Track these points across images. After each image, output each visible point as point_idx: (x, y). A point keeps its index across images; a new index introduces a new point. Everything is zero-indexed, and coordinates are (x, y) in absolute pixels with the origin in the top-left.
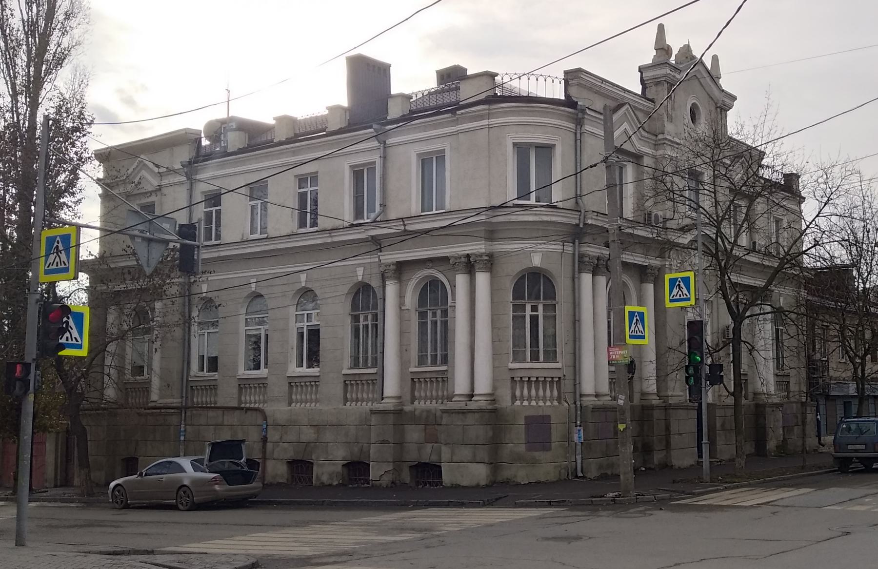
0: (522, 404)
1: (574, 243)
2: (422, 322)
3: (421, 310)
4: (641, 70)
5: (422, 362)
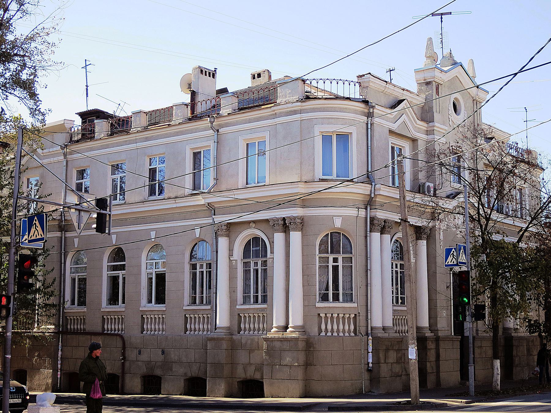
0: (326, 334)
1: (366, 209)
2: (246, 270)
3: (246, 261)
4: (417, 71)
5: (246, 300)
